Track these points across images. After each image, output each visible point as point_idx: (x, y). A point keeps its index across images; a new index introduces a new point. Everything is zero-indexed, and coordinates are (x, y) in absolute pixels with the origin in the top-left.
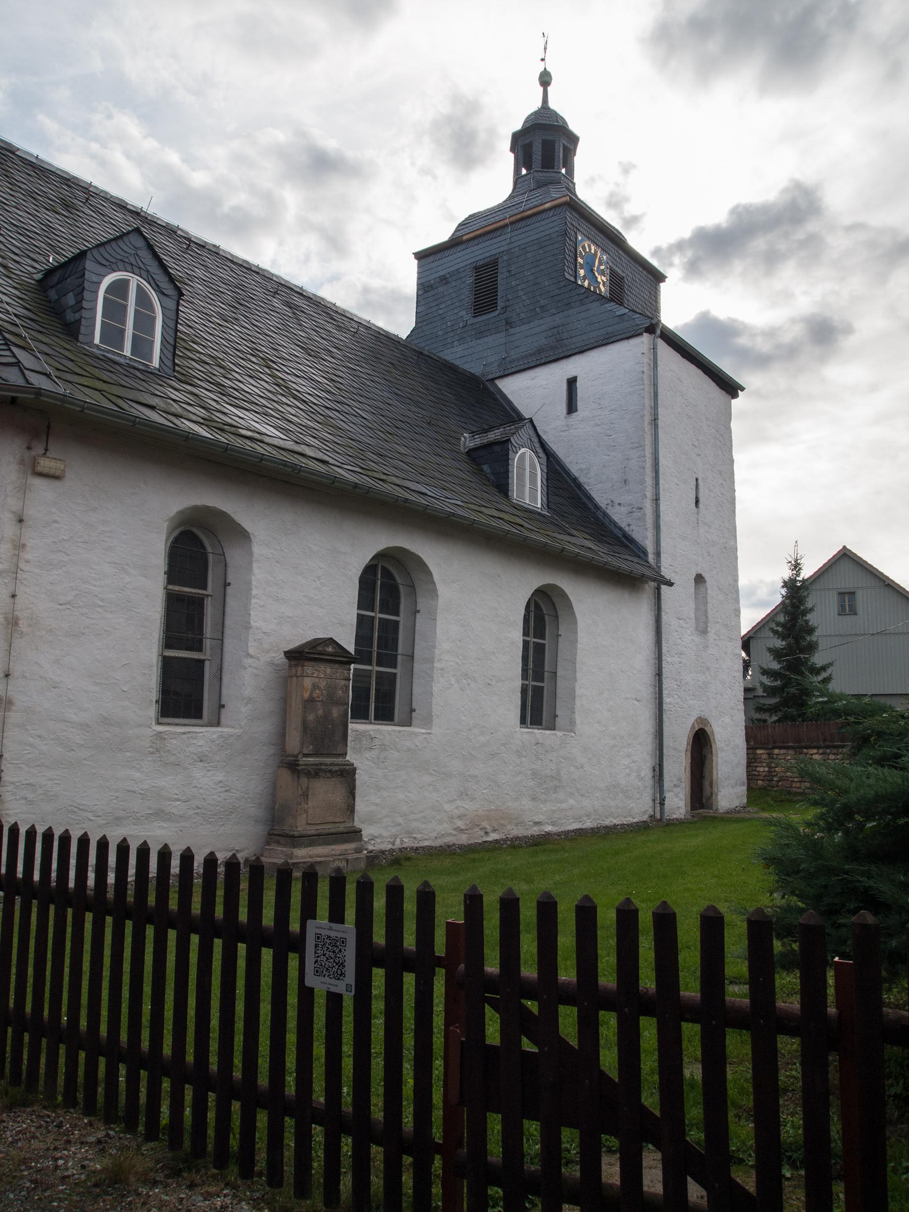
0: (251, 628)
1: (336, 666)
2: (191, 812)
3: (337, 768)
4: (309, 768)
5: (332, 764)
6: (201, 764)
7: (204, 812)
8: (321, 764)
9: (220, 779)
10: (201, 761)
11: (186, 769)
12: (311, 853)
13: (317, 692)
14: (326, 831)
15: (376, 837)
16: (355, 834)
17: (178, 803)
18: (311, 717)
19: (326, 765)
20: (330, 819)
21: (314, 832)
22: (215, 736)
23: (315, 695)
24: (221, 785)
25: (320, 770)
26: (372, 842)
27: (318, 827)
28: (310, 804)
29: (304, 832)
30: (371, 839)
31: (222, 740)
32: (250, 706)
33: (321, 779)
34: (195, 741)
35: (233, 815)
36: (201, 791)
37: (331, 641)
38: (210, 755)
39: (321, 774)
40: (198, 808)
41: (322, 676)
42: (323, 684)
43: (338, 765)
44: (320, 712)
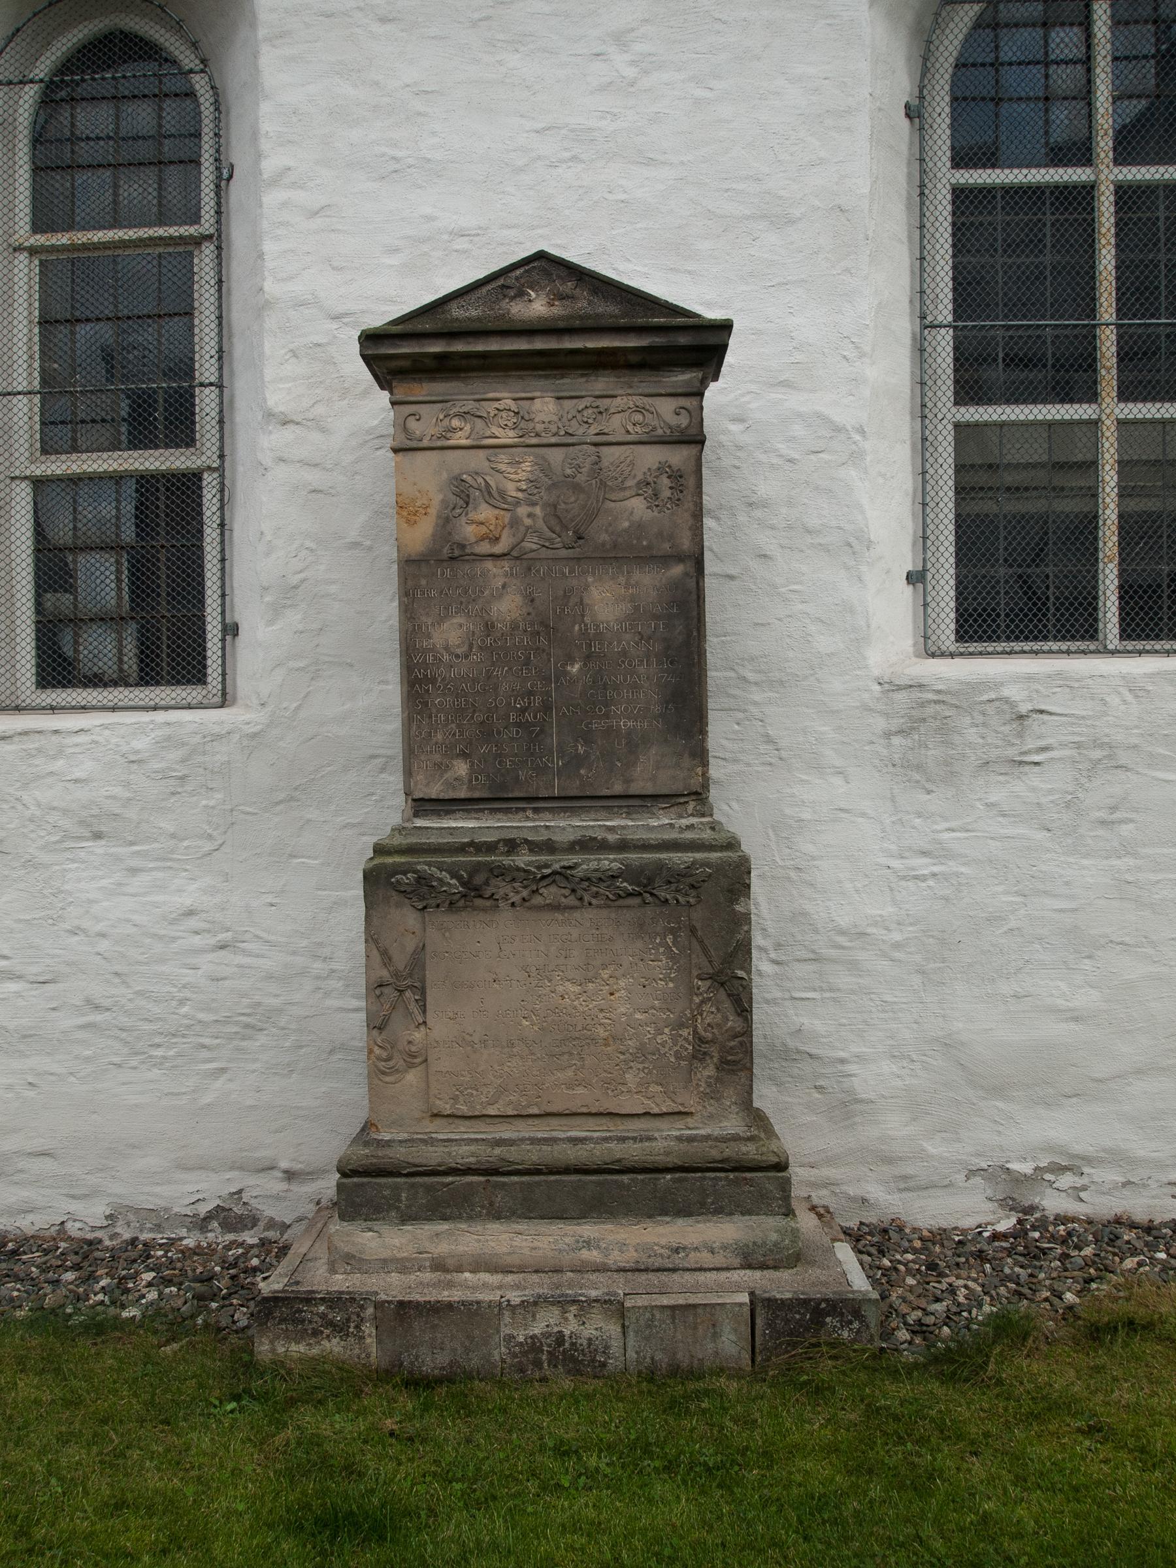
0: (267, 305)
1: (601, 383)
2: (66, 1021)
3: (609, 862)
4: (423, 864)
5: (585, 845)
6: (99, 847)
7: (125, 1021)
8: (512, 846)
9: (187, 901)
10: (98, 836)
11: (31, 864)
12: (443, 1248)
13: (485, 512)
14: (533, 1155)
15: (1088, 1160)
16: (750, 1176)
17: (13, 987)
18: (450, 634)
19: (549, 847)
20: (581, 1098)
21: (464, 1155)
22: (141, 744)
23: (468, 532)
24: (193, 923)
25: (500, 872)
26: (1066, 1180)
27: (506, 1132)
28: (440, 1027)
29: (400, 1154)
30: (1061, 1169)
31: (174, 755)
32: (293, 618)
33: (506, 915)
34: (60, 764)
35: (262, 1039)
36: (104, 945)
37: (544, 267)
38: (132, 814)
39: (501, 887)
40: (97, 1008)
41: (508, 437)
42: (515, 475)
43: (623, 846)
44: (508, 607)
